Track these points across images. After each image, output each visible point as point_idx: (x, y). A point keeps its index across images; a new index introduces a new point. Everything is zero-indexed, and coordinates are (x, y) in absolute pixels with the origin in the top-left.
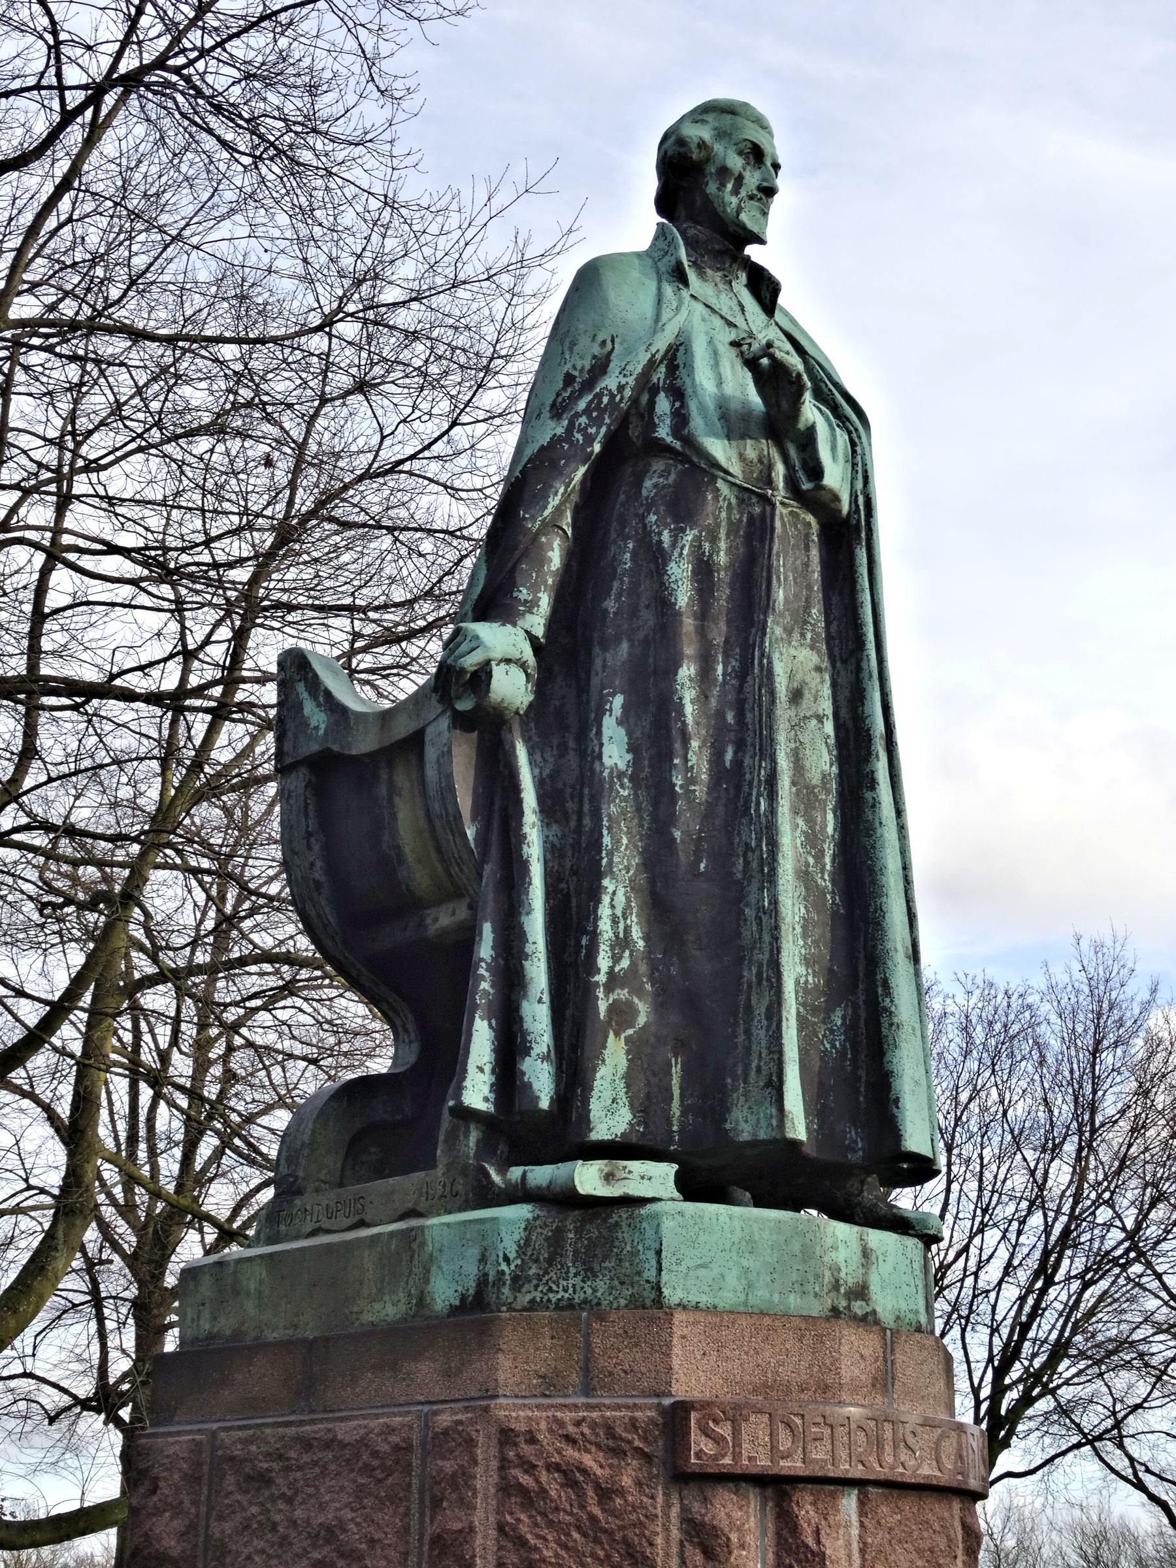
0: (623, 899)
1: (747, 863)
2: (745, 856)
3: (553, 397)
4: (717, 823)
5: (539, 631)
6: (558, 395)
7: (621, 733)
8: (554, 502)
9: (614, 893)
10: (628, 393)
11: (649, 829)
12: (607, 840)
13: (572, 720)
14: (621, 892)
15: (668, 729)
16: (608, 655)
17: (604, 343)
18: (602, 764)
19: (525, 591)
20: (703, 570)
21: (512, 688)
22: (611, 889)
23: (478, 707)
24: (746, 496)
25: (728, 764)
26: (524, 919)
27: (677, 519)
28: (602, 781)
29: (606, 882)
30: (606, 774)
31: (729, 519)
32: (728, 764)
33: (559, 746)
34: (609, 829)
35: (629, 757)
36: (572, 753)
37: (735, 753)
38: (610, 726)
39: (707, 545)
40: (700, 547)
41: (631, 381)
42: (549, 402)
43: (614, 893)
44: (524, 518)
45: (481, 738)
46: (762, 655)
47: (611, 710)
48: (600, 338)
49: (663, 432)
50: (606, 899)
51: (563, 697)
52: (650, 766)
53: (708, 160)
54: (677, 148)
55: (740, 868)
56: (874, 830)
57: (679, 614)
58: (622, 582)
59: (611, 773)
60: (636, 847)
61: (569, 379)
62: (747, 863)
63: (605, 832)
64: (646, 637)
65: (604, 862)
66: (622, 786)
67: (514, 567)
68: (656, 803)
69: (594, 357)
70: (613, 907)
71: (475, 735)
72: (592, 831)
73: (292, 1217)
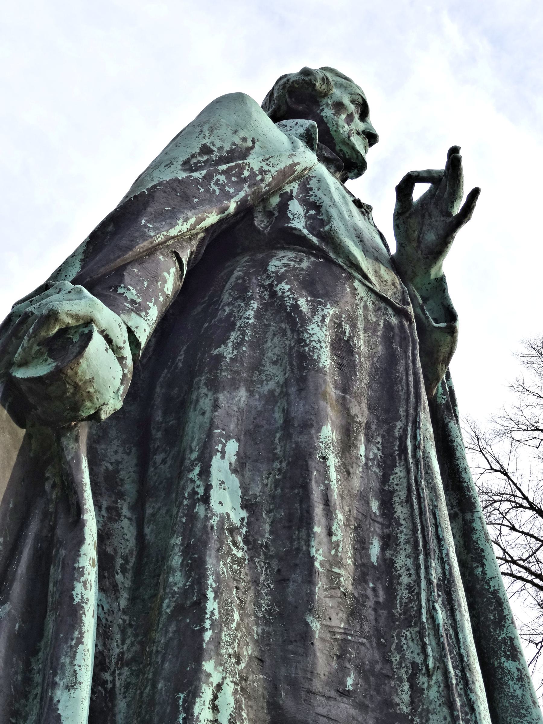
0: (232, 700)
1: (416, 691)
2: (412, 679)
3: (188, 156)
4: (366, 628)
5: (143, 338)
6: (193, 156)
7: (234, 481)
8: (181, 227)
9: (219, 687)
10: (268, 178)
11: (269, 612)
12: (212, 605)
13: (130, 487)
14: (229, 688)
15: (306, 488)
16: (221, 396)
17: (244, 139)
18: (208, 508)
19: (134, 291)
20: (343, 348)
21: (106, 374)
22: (216, 679)
23: (57, 375)
24: (383, 305)
25: (374, 559)
26: (59, 694)
27: (314, 294)
28: (206, 530)
29: (208, 666)
30: (214, 521)
31: (366, 318)
32: (374, 559)
33: (108, 509)
34: (217, 593)
35: (244, 514)
36: (125, 523)
37: (383, 549)
38: (220, 467)
39: (347, 327)
40: (340, 325)
41: (273, 171)
42: (185, 158)
43: (219, 687)
44: (145, 226)
45: (28, 437)
46: (416, 447)
47: (223, 453)
48: (242, 134)
49: (299, 224)
50: (207, 693)
51: (118, 463)
52: (271, 533)
53: (326, 95)
54: (302, 77)
55: (406, 697)
56: (527, 709)
57: (320, 371)
58: (243, 333)
59: (221, 522)
60: (249, 632)
61: (206, 150)
62: (416, 691)
63: (210, 595)
64: (271, 392)
65: (208, 635)
66: (235, 543)
67: (124, 267)
68: (281, 581)
69: (234, 144)
70: (215, 708)
71: (22, 432)
72: (186, 592)
73: (330, 673)
